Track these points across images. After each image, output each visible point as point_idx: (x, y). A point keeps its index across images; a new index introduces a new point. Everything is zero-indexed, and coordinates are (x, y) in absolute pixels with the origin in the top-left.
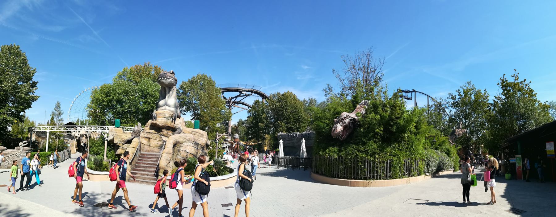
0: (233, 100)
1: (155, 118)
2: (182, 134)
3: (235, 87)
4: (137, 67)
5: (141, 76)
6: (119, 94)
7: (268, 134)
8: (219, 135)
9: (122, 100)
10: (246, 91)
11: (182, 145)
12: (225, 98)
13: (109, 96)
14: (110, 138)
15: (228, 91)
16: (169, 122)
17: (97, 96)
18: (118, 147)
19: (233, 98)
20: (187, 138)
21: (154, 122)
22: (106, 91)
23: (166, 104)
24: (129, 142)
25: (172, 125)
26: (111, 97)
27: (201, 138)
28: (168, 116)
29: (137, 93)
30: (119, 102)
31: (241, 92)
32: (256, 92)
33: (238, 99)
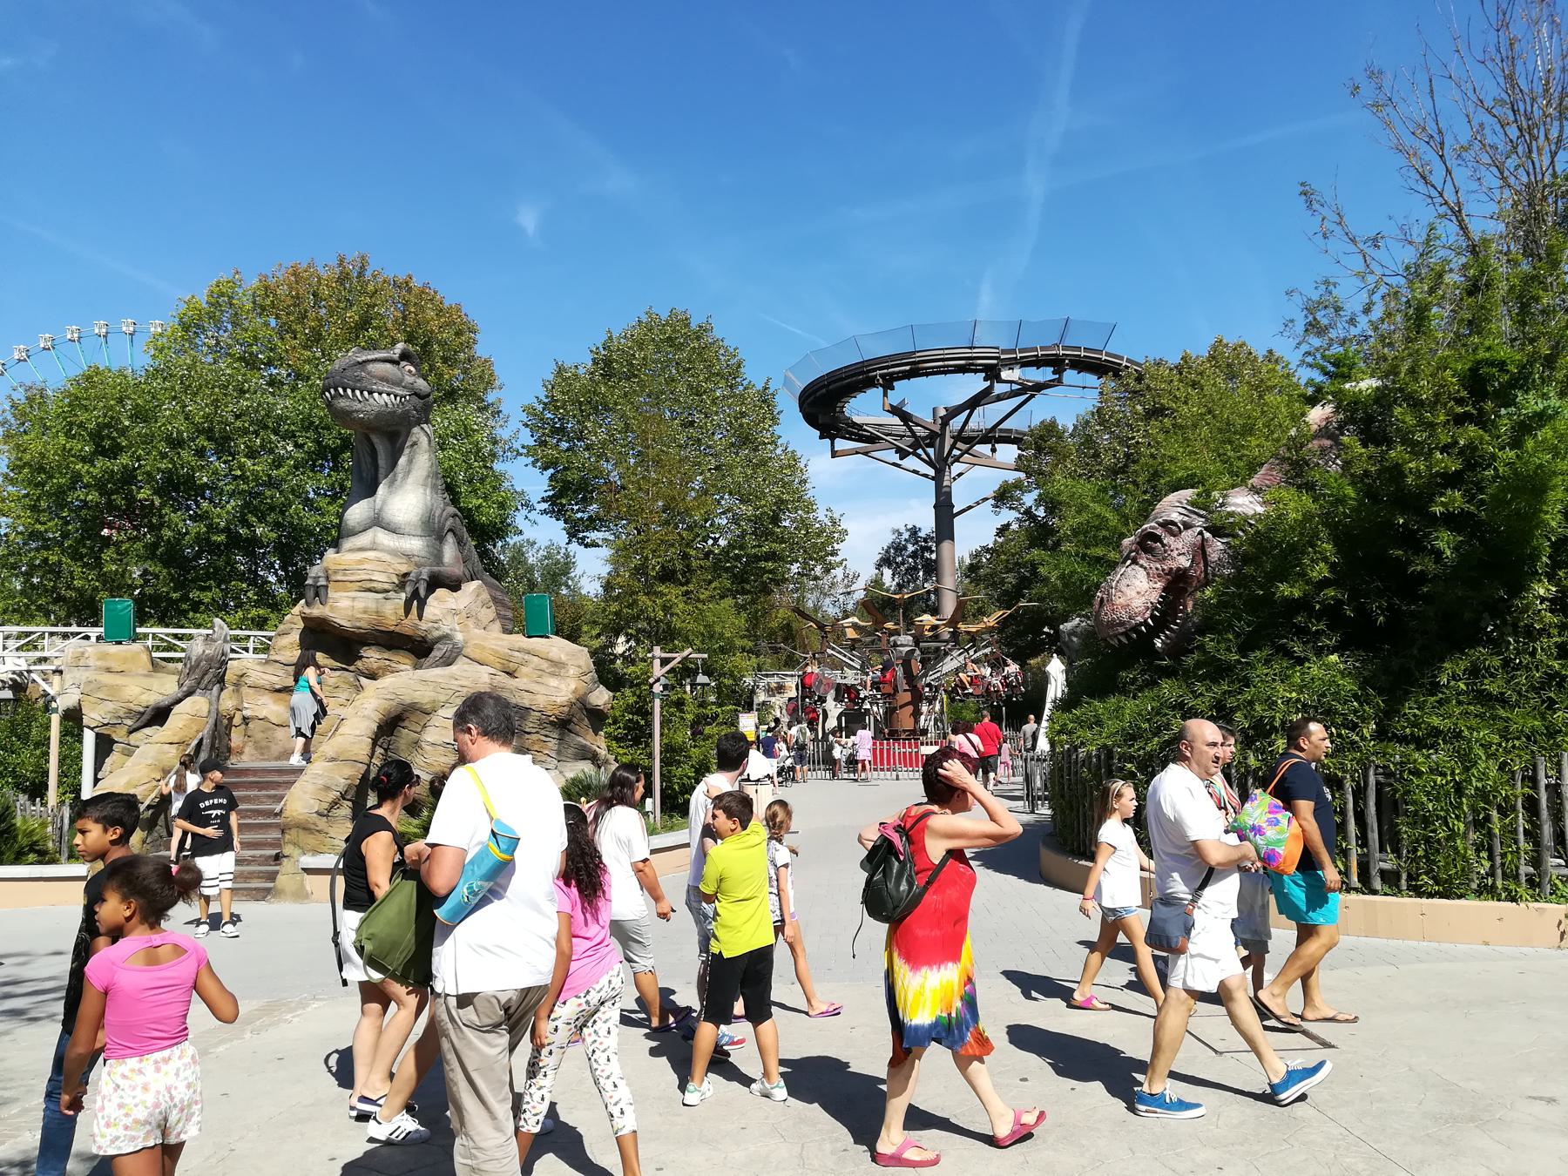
1: (319, 593)
2: (460, 667)
5: (316, 338)
6: (176, 443)
7: (1187, 618)
8: (664, 662)
9: (190, 478)
10: (1025, 363)
12: (906, 418)
13: (114, 452)
15: (915, 372)
16: (391, 611)
17: (50, 446)
19: (953, 412)
20: (454, 684)
21: (317, 611)
22: (91, 419)
23: (377, 521)
24: (159, 715)
25: (410, 625)
26: (124, 459)
27: (553, 682)
28: (382, 578)
29: (290, 436)
30: (178, 487)
31: (992, 373)
32: (1082, 365)
33: (984, 418)
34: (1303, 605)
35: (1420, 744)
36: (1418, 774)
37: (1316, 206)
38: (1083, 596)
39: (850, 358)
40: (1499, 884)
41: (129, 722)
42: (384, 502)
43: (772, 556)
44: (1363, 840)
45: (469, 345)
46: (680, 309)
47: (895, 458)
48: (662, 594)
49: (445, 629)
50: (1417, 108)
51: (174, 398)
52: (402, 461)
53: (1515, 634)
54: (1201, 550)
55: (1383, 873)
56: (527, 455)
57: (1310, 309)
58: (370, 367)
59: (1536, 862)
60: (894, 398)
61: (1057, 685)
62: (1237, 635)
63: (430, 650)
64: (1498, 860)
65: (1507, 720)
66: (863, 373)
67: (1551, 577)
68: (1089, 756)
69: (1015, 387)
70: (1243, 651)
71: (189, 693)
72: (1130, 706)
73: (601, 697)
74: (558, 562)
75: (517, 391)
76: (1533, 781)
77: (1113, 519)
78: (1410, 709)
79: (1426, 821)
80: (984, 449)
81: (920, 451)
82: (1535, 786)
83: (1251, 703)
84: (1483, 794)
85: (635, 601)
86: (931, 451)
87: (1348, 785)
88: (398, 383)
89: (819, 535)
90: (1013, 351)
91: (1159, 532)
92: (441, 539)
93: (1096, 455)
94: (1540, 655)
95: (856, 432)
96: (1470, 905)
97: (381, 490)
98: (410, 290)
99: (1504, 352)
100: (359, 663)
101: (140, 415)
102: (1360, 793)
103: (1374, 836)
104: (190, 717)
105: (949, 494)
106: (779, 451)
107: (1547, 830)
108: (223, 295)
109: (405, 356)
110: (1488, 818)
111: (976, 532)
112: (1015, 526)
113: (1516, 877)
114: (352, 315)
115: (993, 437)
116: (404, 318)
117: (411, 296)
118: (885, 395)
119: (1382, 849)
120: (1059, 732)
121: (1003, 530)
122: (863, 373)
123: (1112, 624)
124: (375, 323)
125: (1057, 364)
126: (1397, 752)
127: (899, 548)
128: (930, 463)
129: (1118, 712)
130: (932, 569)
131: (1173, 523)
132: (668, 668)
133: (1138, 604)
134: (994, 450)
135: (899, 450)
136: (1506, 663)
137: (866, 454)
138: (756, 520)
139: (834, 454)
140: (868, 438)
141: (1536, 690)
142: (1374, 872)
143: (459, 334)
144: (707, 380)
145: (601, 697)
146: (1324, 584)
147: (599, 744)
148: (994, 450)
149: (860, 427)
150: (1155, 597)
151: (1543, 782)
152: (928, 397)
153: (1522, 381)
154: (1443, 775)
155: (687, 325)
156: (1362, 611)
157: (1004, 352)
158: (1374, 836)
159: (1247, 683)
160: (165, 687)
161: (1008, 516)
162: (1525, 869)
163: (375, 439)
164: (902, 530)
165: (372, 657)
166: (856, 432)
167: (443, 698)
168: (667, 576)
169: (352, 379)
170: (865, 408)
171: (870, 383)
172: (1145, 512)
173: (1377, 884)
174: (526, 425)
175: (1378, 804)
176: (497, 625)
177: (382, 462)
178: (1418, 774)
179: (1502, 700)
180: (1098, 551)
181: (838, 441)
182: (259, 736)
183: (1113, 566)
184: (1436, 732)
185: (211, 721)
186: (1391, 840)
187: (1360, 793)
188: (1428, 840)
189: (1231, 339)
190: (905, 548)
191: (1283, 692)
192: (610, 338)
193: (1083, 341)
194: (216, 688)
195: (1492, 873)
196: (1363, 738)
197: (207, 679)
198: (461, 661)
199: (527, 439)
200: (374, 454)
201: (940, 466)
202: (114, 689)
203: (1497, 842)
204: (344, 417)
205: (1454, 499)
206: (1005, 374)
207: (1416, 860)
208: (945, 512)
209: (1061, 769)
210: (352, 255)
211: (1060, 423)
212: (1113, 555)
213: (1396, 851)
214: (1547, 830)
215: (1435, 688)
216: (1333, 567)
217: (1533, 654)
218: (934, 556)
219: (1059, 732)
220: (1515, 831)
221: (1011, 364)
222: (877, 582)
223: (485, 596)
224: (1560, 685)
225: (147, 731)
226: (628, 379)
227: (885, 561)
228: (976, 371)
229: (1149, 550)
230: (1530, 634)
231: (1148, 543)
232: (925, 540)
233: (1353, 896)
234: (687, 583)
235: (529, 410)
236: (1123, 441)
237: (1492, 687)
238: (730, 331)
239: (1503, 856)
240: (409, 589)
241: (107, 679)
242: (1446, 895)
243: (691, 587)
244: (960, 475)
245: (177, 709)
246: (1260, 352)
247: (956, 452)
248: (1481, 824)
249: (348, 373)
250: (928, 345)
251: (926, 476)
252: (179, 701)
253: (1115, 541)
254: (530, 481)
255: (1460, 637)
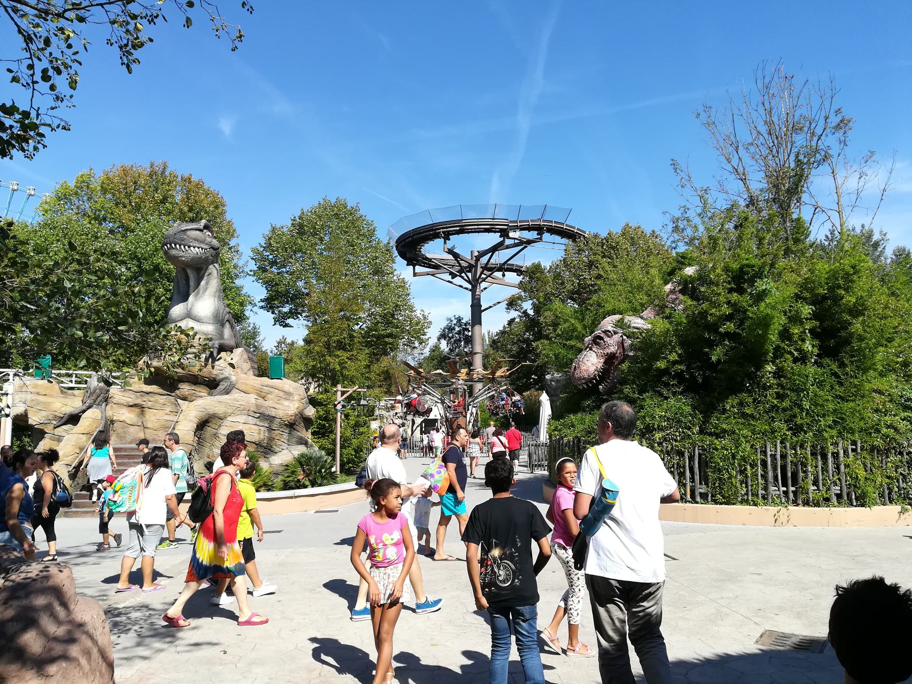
0: (484, 260)
2: (235, 394)
3: (487, 216)
4: (125, 172)
5: (138, 208)
8: (343, 393)
11: (226, 423)
12: (456, 256)
14: (19, 409)
15: (462, 231)
18: (41, 434)
19: (482, 254)
23: (189, 315)
24: (73, 419)
25: (207, 372)
27: (286, 403)
29: (123, 263)
31: (504, 233)
32: (553, 231)
33: (500, 257)
34: (665, 372)
35: (718, 436)
36: (717, 449)
37: (678, 171)
38: (565, 365)
39: (426, 221)
40: (750, 498)
41: (54, 422)
42: (193, 305)
43: (390, 335)
44: (692, 479)
45: (223, 213)
46: (342, 197)
47: (449, 278)
48: (338, 356)
49: (226, 374)
50: (727, 129)
51: (58, 240)
52: (203, 283)
53: (758, 387)
54: (621, 344)
55: (701, 494)
56: (254, 275)
57: (675, 221)
58: (188, 233)
59: (766, 488)
60: (449, 244)
61: (546, 411)
62: (638, 386)
63: (218, 385)
64: (750, 488)
65: (754, 426)
66: (432, 230)
67: (773, 362)
68: (569, 441)
69: (517, 241)
70: (640, 393)
71: (89, 407)
72: (588, 418)
73: (311, 412)
74: (249, 332)
75: (247, 242)
76: (764, 453)
77: (579, 327)
78: (714, 421)
79: (720, 471)
80: (498, 274)
81: (463, 275)
82: (766, 456)
83: (644, 417)
84: (744, 459)
85: (325, 360)
86: (469, 275)
87: (686, 455)
88: (203, 242)
89: (417, 324)
90: (516, 222)
91: (603, 335)
92: (223, 325)
93: (563, 283)
94: (769, 398)
95: (428, 263)
96: (738, 507)
97: (191, 298)
98: (190, 182)
99: (753, 261)
100: (177, 392)
101: (38, 250)
102: (691, 458)
103: (697, 477)
104: (91, 419)
105: (479, 299)
106: (395, 278)
107: (770, 474)
108: (83, 182)
109: (206, 227)
110: (746, 469)
111: (495, 321)
112: (518, 320)
113: (757, 495)
114: (158, 196)
115: (504, 268)
116: (188, 198)
117: (192, 188)
118: (445, 243)
119: (701, 483)
120: (554, 430)
121: (511, 322)
122: (432, 230)
123: (580, 379)
124: (170, 200)
125: (540, 229)
126: (708, 440)
127: (451, 329)
128: (469, 282)
129: (582, 421)
130: (469, 340)
131: (609, 331)
132: (345, 396)
133: (592, 369)
134: (504, 275)
135: (451, 273)
136: (755, 400)
137: (433, 275)
138: (384, 316)
139: (415, 275)
140: (434, 266)
141: (765, 412)
142: (697, 493)
143: (217, 207)
144: (358, 238)
145: (311, 412)
146: (675, 363)
147: (308, 436)
148: (504, 275)
149: (430, 260)
150: (600, 366)
151: (769, 453)
152: (470, 245)
153: (759, 275)
154: (727, 450)
155: (346, 207)
156: (692, 375)
157: (511, 222)
158: (697, 477)
159: (642, 407)
160: (73, 404)
161: (514, 314)
162: (761, 492)
163: (189, 271)
164: (453, 319)
165: (185, 388)
166: (428, 263)
167: (230, 411)
168: (341, 346)
169: (179, 239)
170: (433, 250)
171: (437, 236)
172: (595, 324)
173: (698, 499)
174: (253, 259)
175: (699, 463)
176: (251, 373)
177: (192, 283)
178: (717, 449)
179: (752, 417)
180: (572, 343)
181: (417, 267)
182: (120, 431)
183: (580, 351)
184: (724, 431)
185: (103, 422)
186: (704, 479)
187: (691, 458)
188: (720, 479)
189: (633, 225)
190: (454, 329)
191: (658, 412)
192: (303, 213)
193: (554, 218)
194: (104, 404)
195: (747, 494)
196: (693, 434)
197: (99, 399)
198: (234, 391)
199: (253, 266)
200: (187, 279)
201: (474, 283)
202: (47, 404)
203: (749, 480)
204: (173, 259)
205: (730, 326)
206: (511, 234)
207: (715, 488)
208: (477, 309)
209: (555, 448)
210: (158, 162)
211: (543, 265)
212: (579, 345)
213: (707, 484)
214: (770, 474)
215: (724, 411)
216: (679, 355)
217: (766, 397)
218: (470, 334)
219: (554, 430)
220: (757, 475)
221: (515, 228)
222: (436, 348)
223: (245, 356)
224: (777, 411)
225: (64, 427)
226: (313, 236)
227: (443, 336)
228: (495, 232)
229: (597, 344)
230: (765, 388)
231: (597, 341)
232: (465, 325)
233: (688, 504)
234: (351, 350)
235: (254, 250)
236: (578, 277)
237: (748, 411)
238: (367, 212)
239: (752, 486)
240: (208, 353)
241: (41, 398)
242: (728, 503)
243: (355, 353)
244: (485, 289)
245: (84, 416)
246: (648, 232)
247: (483, 276)
248: (743, 472)
249: (177, 236)
250: (470, 215)
251: (466, 289)
252: (84, 411)
253: (581, 338)
254: (256, 291)
255: (735, 388)
